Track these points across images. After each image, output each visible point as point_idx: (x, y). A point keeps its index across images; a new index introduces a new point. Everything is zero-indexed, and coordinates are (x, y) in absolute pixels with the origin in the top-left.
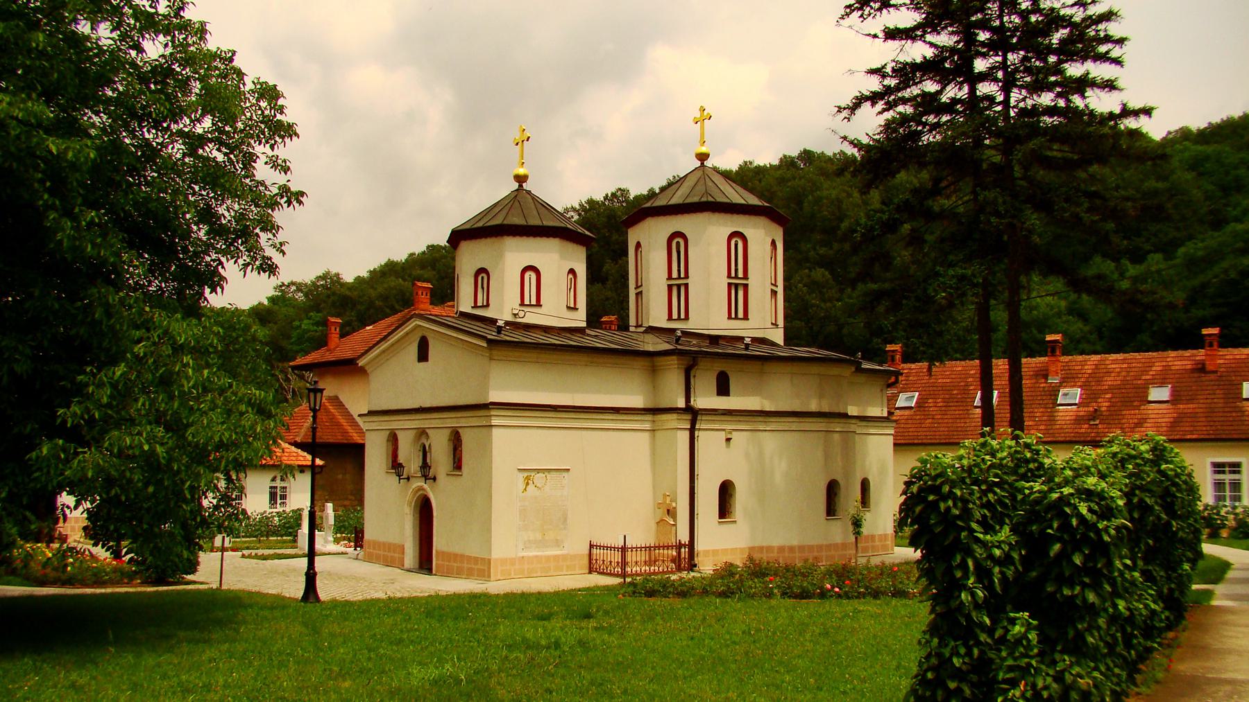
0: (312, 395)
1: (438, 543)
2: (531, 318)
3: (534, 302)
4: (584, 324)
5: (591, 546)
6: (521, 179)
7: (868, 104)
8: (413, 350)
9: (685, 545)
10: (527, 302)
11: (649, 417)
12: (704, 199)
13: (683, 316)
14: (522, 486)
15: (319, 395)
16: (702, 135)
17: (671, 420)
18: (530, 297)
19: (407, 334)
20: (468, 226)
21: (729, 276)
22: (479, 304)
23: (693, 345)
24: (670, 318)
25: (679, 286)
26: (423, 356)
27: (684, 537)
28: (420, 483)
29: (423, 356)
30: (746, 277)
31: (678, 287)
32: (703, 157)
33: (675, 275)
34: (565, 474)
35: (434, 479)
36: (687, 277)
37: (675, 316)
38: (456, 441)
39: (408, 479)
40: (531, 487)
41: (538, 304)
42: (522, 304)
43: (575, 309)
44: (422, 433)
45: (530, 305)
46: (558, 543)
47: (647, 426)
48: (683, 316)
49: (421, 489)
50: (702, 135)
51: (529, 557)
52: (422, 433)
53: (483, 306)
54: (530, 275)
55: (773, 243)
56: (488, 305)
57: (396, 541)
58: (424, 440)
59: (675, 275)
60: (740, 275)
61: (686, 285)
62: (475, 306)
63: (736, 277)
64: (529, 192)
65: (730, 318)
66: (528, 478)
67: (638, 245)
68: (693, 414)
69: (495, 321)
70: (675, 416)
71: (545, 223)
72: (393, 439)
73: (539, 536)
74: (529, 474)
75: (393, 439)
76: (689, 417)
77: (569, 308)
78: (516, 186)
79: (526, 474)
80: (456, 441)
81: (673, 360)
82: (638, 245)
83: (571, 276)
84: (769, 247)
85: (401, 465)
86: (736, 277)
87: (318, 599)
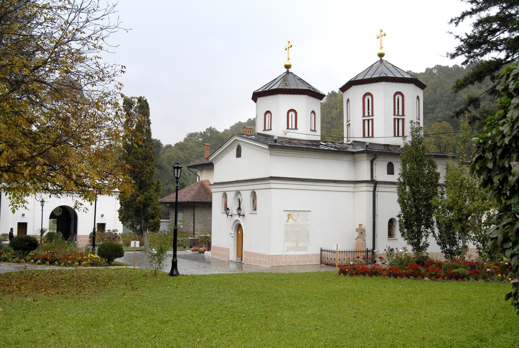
0: (176, 170)
1: (246, 248)
2: (292, 135)
3: (294, 127)
4: (319, 138)
5: (322, 250)
6: (288, 67)
7: (469, 16)
8: (234, 152)
9: (370, 251)
10: (290, 127)
11: (352, 185)
12: (381, 76)
13: (370, 135)
14: (286, 219)
15: (179, 170)
16: (381, 44)
17: (364, 187)
18: (292, 124)
19: (231, 144)
20: (261, 90)
21: (394, 114)
22: (267, 129)
23: (376, 149)
24: (364, 136)
25: (368, 120)
26: (239, 155)
27: (370, 247)
28: (237, 217)
29: (239, 155)
30: (403, 114)
31: (368, 122)
32: (381, 55)
33: (366, 114)
34: (308, 213)
35: (244, 216)
36: (373, 115)
37: (366, 135)
38: (254, 194)
39: (232, 216)
40: (291, 220)
41: (296, 128)
42: (288, 128)
43: (315, 131)
44: (238, 193)
45: (292, 129)
46: (304, 249)
47: (351, 189)
48: (370, 135)
49: (237, 221)
50: (381, 44)
51: (289, 255)
52: (238, 193)
53: (268, 130)
54: (292, 114)
55: (418, 97)
56: (271, 129)
57: (226, 247)
58: (239, 197)
59: (366, 114)
60: (400, 113)
61: (372, 120)
62: (265, 130)
63: (398, 115)
64: (292, 73)
65: (395, 136)
66: (289, 215)
67: (348, 100)
68: (374, 183)
69: (273, 137)
70: (365, 185)
71: (299, 88)
72: (225, 195)
73: (294, 244)
74: (290, 214)
75: (225, 195)
76: (373, 185)
77: (311, 130)
78: (285, 70)
79: (288, 213)
80: (254, 194)
81: (364, 157)
82: (348, 100)
83: (312, 114)
84: (415, 100)
85: (228, 209)
86: (398, 115)
87: (178, 274)
